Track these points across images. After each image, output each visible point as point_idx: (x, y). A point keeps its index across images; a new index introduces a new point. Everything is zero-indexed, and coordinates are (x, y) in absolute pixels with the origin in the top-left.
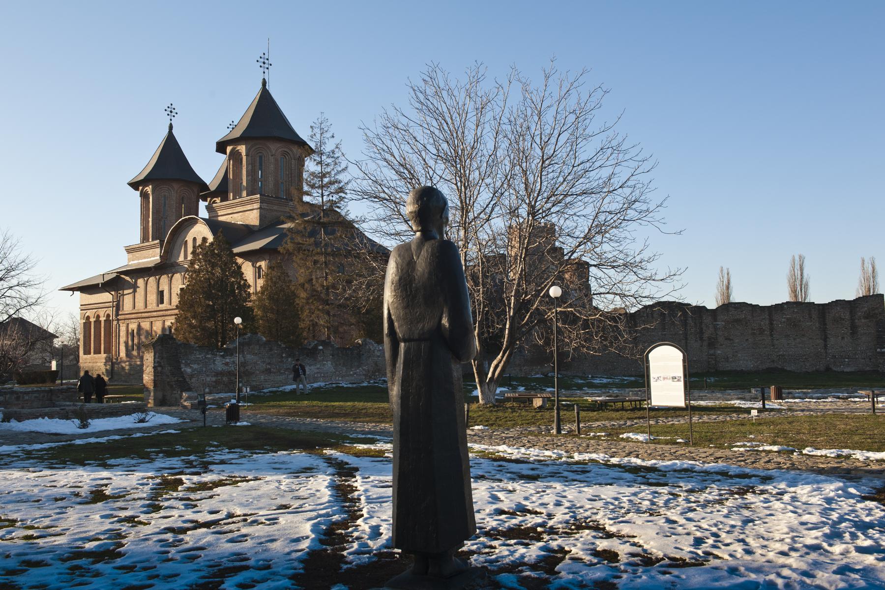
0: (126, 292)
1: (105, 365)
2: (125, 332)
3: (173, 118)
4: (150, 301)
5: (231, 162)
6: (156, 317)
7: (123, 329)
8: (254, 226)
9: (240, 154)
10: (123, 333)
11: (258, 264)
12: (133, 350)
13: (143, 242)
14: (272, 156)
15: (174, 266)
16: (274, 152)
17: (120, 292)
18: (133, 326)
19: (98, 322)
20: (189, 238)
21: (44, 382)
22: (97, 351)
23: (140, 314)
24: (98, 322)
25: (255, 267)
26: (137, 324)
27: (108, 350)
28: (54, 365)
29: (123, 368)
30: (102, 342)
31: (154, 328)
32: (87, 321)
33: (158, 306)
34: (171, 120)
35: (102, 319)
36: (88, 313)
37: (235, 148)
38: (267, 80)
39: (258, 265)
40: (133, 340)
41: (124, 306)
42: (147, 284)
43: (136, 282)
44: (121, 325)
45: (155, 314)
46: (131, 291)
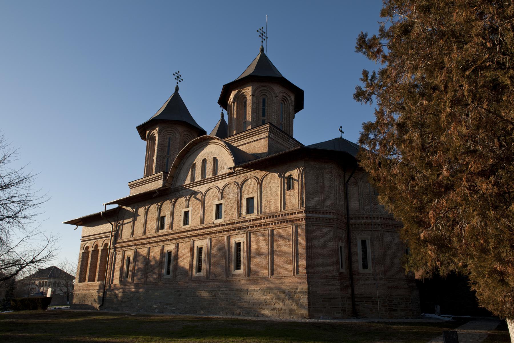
0: (125, 221)
1: (98, 292)
2: (121, 260)
3: (179, 82)
4: (150, 228)
5: (235, 105)
6: (154, 242)
7: (119, 256)
8: (261, 154)
9: (245, 97)
10: (118, 261)
11: (287, 174)
12: (127, 277)
13: (146, 176)
14: (276, 97)
15: (179, 191)
16: (277, 93)
17: (120, 222)
18: (130, 253)
19: (96, 251)
20: (198, 161)
21: (35, 308)
22: (92, 279)
23: (138, 241)
24: (96, 251)
25: (284, 177)
26: (133, 251)
27: (102, 278)
28: (49, 292)
29: (116, 295)
30: (98, 270)
31: (152, 254)
32: (86, 251)
33: (158, 231)
34: (177, 83)
35: (100, 248)
36: (88, 244)
37: (240, 92)
38: (265, 48)
39: (287, 174)
40: (128, 267)
41: (123, 234)
42: (147, 212)
43: (137, 211)
44: (118, 253)
45: (154, 240)
46: (130, 220)
